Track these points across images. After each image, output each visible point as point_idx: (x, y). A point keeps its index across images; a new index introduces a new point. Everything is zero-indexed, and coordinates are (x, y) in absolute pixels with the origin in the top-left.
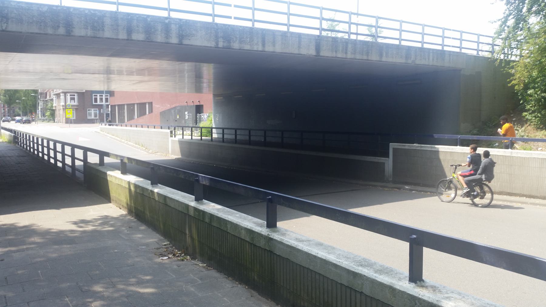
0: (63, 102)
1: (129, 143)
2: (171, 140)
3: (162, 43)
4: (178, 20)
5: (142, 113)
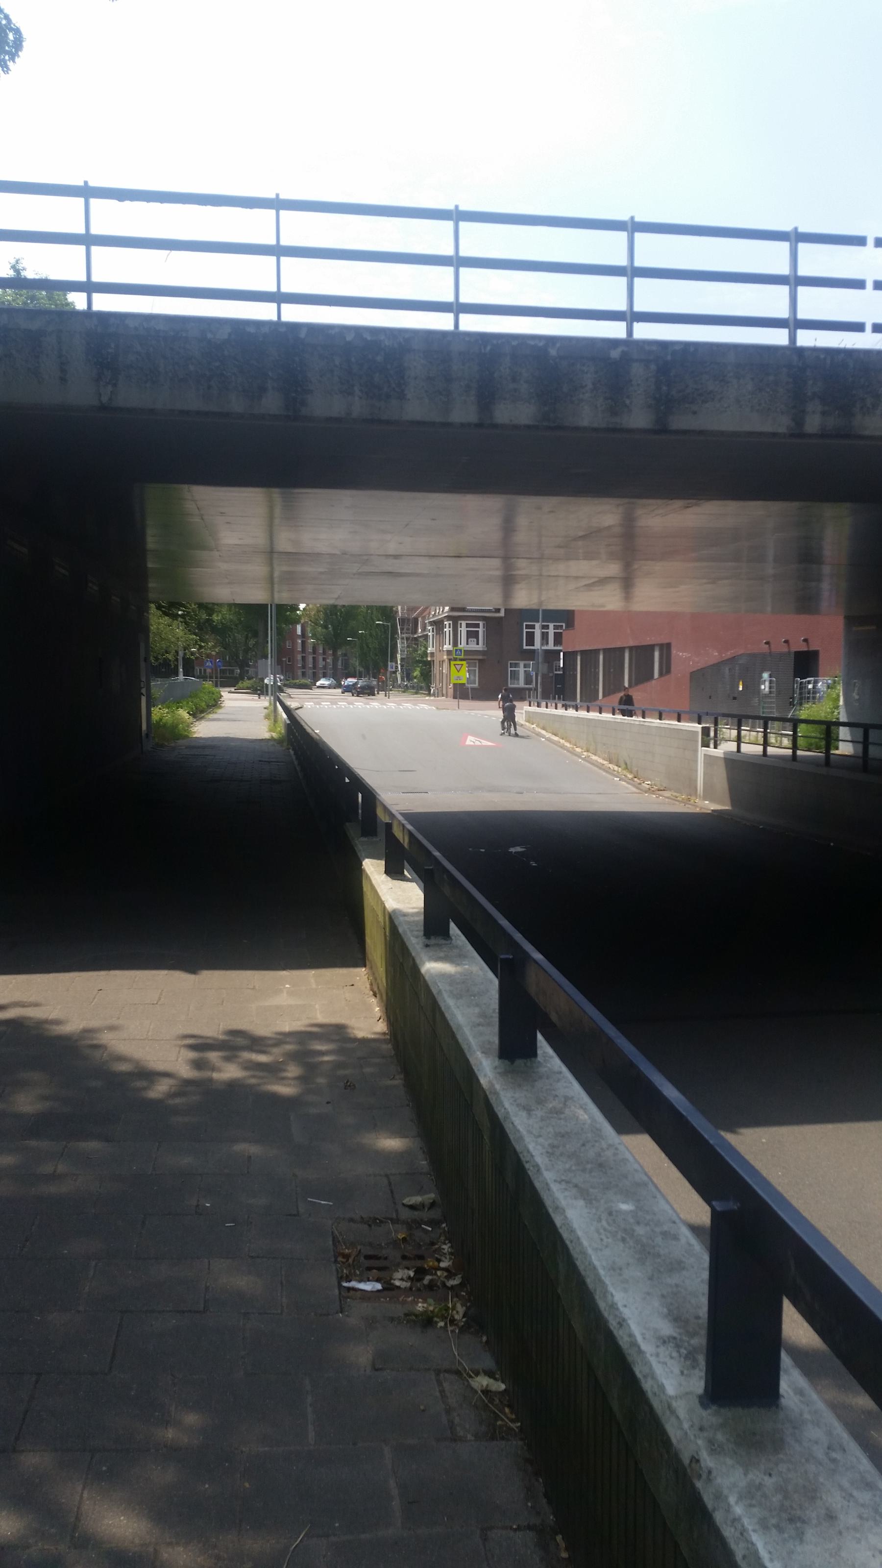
0: (450, 644)
1: (594, 758)
2: (703, 756)
3: (595, 430)
4: (654, 348)
5: (643, 675)
